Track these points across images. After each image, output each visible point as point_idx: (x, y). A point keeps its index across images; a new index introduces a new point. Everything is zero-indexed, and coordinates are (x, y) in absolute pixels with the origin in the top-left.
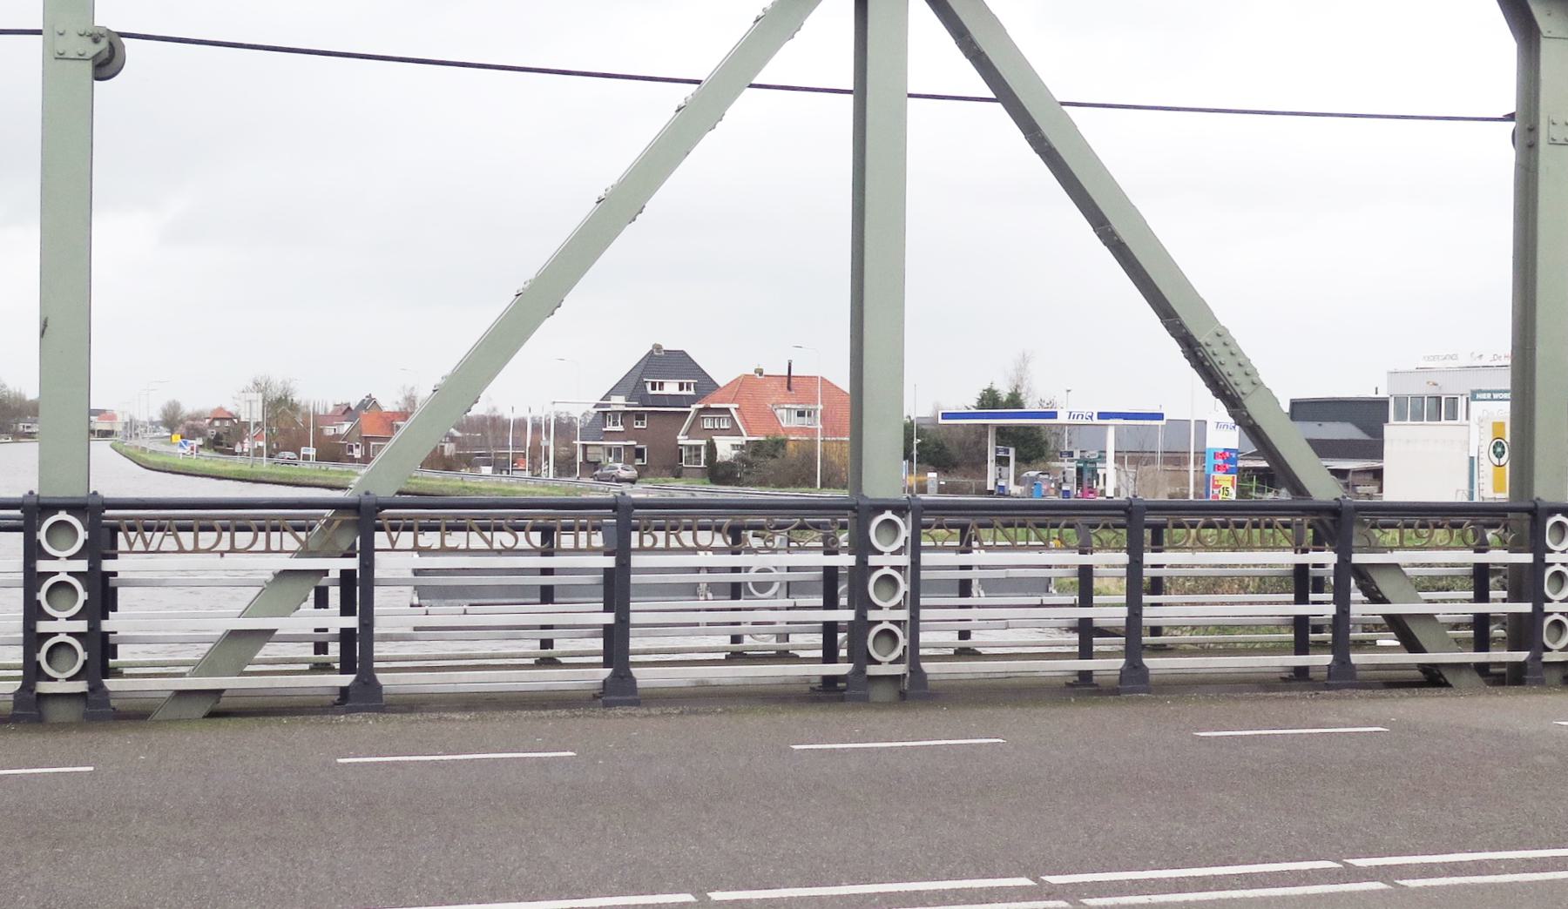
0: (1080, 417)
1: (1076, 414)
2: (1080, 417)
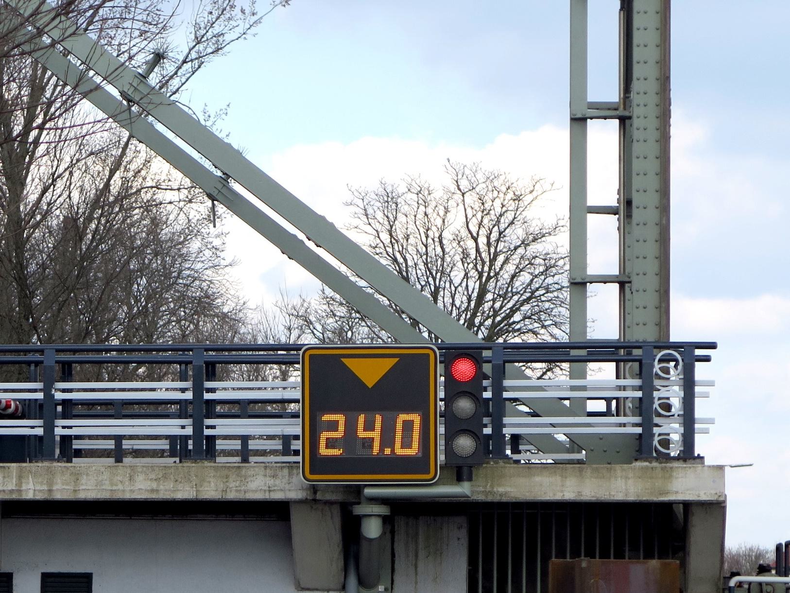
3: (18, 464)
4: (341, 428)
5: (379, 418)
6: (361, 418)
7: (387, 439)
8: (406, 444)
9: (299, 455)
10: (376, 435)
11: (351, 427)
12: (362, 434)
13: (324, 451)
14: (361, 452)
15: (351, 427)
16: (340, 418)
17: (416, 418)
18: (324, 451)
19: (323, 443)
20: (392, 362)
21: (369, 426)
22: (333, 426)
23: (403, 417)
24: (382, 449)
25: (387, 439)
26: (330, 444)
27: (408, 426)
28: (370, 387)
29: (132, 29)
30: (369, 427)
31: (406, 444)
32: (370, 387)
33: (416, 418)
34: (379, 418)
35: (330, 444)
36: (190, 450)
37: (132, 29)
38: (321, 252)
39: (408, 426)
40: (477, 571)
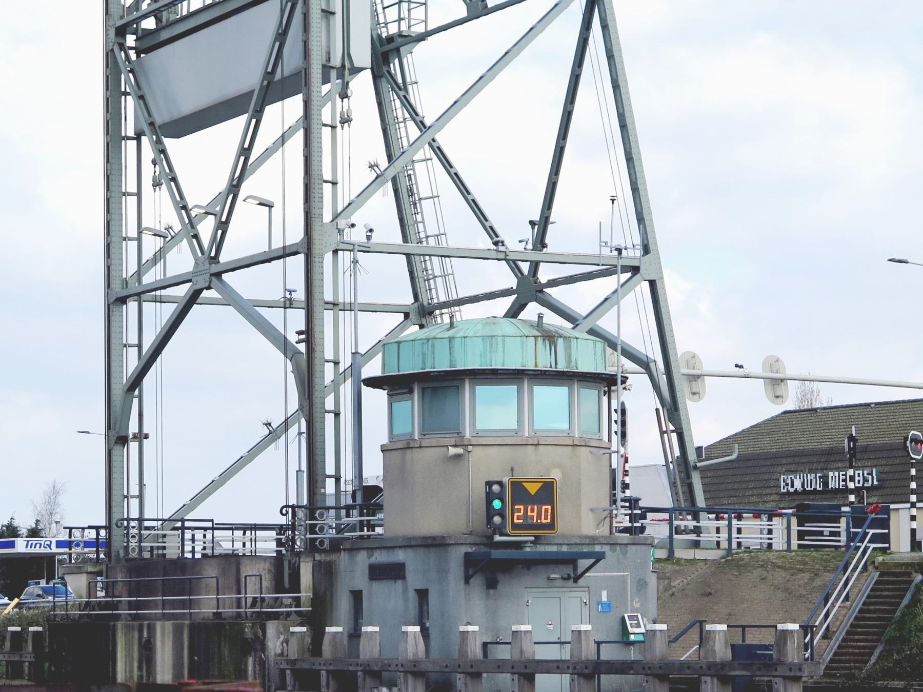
0: (38, 545)
1: (34, 543)
2: (38, 545)
3: (400, 373)
4: (522, 511)
5: (536, 507)
6: (529, 507)
7: (539, 517)
8: (546, 518)
9: (14, 541)
10: (535, 514)
11: (526, 511)
12: (530, 514)
13: (516, 521)
14: (529, 521)
15: (526, 511)
16: (522, 507)
17: (549, 507)
18: (516, 521)
19: (515, 518)
20: (540, 484)
21: (532, 511)
22: (519, 511)
23: (544, 507)
24: (537, 521)
25: (539, 517)
26: (518, 518)
27: (546, 510)
28: (533, 493)
29: (346, 491)
30: (532, 511)
31: (546, 518)
32: (533, 493)
33: (549, 507)
34: (536, 507)
35: (518, 518)
36: (847, 497)
37: (346, 491)
38: (111, 670)
39: (546, 510)
40: (880, 609)
